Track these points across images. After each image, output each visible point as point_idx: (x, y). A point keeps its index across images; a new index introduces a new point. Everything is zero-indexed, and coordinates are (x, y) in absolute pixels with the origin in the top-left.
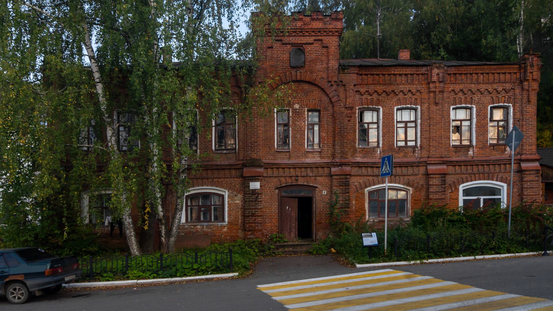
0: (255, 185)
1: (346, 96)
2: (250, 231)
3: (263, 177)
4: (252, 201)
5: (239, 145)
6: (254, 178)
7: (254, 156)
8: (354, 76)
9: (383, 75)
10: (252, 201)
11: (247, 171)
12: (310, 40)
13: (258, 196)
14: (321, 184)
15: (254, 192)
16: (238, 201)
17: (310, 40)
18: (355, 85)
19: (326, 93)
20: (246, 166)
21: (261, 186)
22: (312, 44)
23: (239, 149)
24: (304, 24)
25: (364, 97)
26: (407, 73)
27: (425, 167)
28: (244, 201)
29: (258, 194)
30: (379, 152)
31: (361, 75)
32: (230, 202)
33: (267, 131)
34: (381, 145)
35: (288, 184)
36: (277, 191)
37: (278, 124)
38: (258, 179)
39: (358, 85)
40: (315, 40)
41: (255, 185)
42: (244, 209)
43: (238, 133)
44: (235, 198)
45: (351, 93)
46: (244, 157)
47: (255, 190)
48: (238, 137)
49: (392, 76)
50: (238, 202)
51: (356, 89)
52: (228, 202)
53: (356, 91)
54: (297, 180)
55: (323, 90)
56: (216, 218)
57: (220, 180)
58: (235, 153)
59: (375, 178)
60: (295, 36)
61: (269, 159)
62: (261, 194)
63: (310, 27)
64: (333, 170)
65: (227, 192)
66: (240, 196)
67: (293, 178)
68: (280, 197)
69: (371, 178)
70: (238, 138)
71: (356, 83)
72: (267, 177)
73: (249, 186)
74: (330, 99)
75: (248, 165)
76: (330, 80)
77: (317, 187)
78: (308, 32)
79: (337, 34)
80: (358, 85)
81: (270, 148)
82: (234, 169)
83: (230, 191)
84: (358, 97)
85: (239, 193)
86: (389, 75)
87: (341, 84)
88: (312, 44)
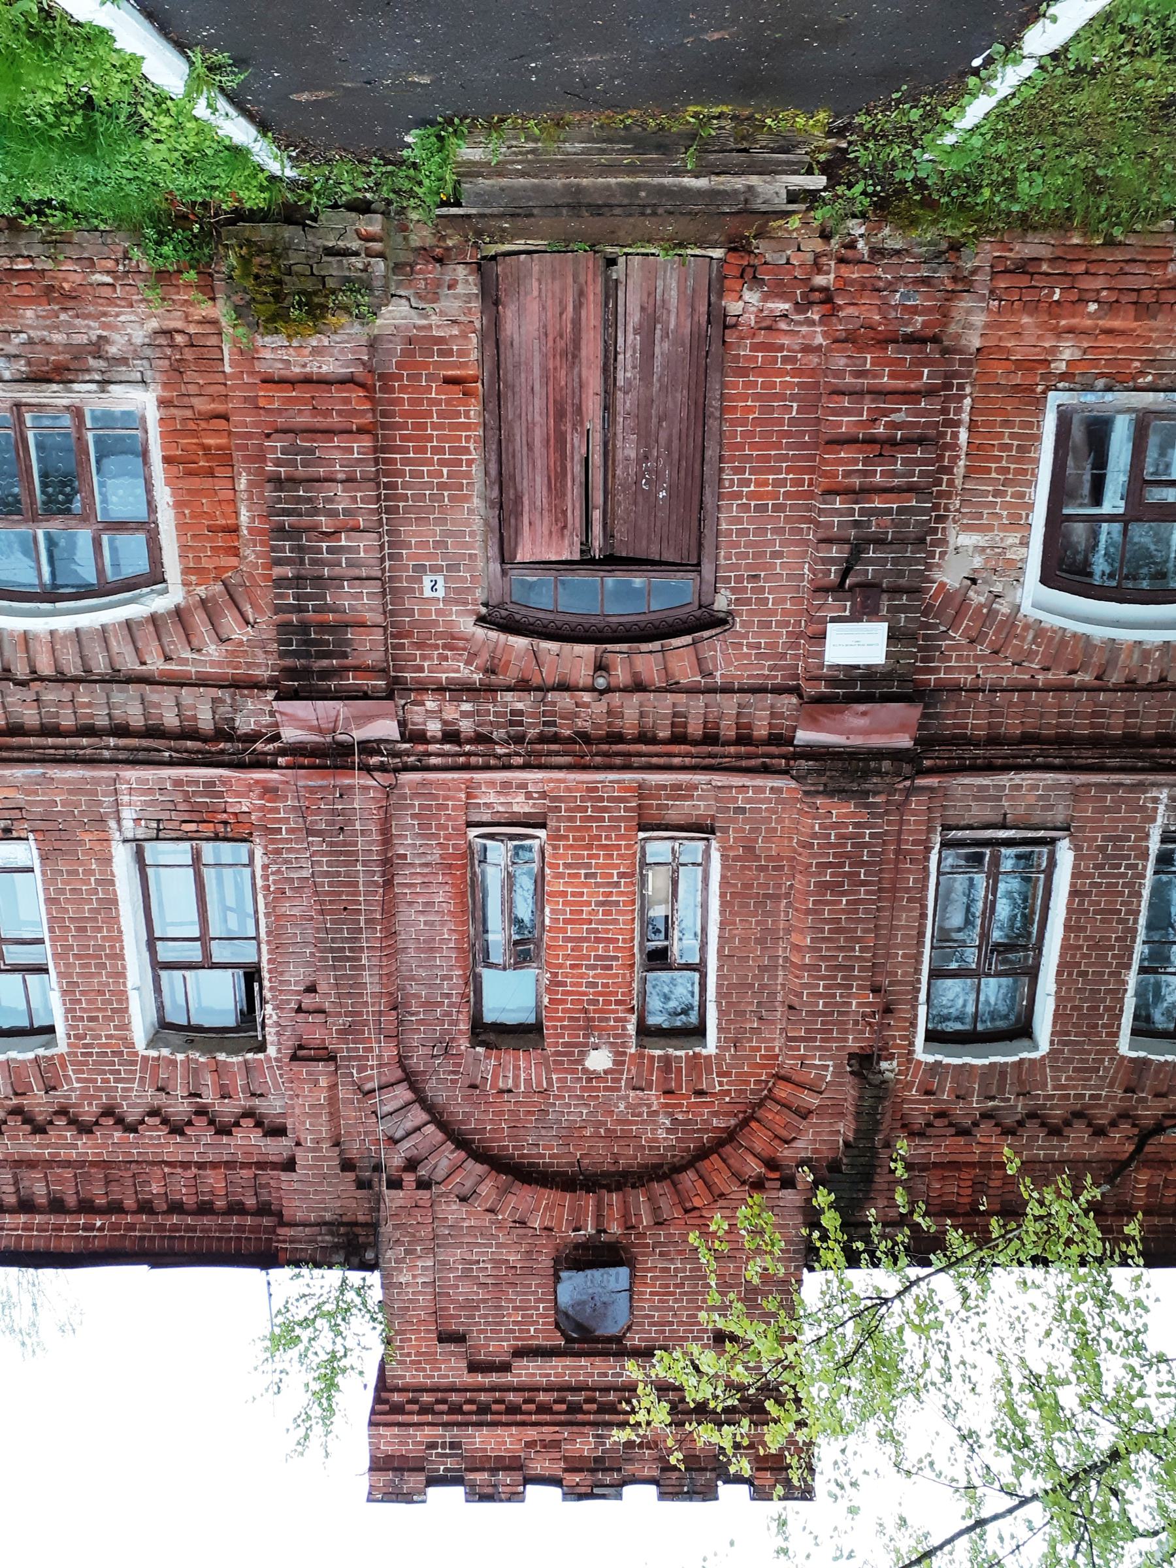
0: (858, 644)
1: (334, 1116)
2: (910, 339)
3: (796, 690)
4: (880, 542)
5: (926, 869)
6: (858, 687)
7: (841, 811)
8: (297, 1208)
9: (145, 1207)
10: (880, 542)
11: (887, 728)
12: (528, 1371)
13: (845, 574)
14: (453, 641)
15: (864, 601)
16: (961, 554)
17: (528, 1371)
18: (289, 1165)
19: (442, 1126)
20: (897, 755)
21: (821, 637)
22: (519, 1353)
23: (928, 850)
24: (555, 1444)
25: (242, 1101)
26: (23, 1218)
27: (59, 582)
28: (924, 540)
29: (838, 588)
30: (127, 814)
31: (263, 1209)
32: (1013, 539)
33: (761, 941)
34: (122, 856)
35: (656, 645)
36: (721, 603)
37: (700, 968)
38: (832, 681)
39: (274, 1166)
40: (505, 1368)
41: (858, 644)
42: (930, 490)
43: (921, 934)
44: (978, 562)
45: (309, 1129)
46: (901, 807)
47: (854, 618)
48: (923, 916)
49: (101, 1201)
50: (967, 540)
51: (284, 1141)
52: (1025, 543)
53: (279, 1131)
54: (601, 667)
55: (461, 1142)
56: (1098, 432)
57: (1058, 675)
58: (946, 828)
59: (129, 663)
60: (606, 1390)
61: (761, 789)
62: (821, 590)
63: (532, 1433)
64: (385, 728)
65: (1027, 609)
66: (949, 575)
67: (621, 675)
68: (707, 568)
69: (155, 664)
70: (924, 907)
71: (284, 1176)
72: (778, 690)
73: (892, 637)
74: (421, 1100)
75: (886, 765)
76: (424, 1194)
77: (481, 620)
78: (543, 1409)
79: (396, 1397)
80: (274, 1166)
81: (749, 849)
82: (968, 741)
83: (1003, 608)
84: (272, 1106)
85: (949, 597)
86: (116, 1208)
87: (361, 1173)
88: (519, 1353)
